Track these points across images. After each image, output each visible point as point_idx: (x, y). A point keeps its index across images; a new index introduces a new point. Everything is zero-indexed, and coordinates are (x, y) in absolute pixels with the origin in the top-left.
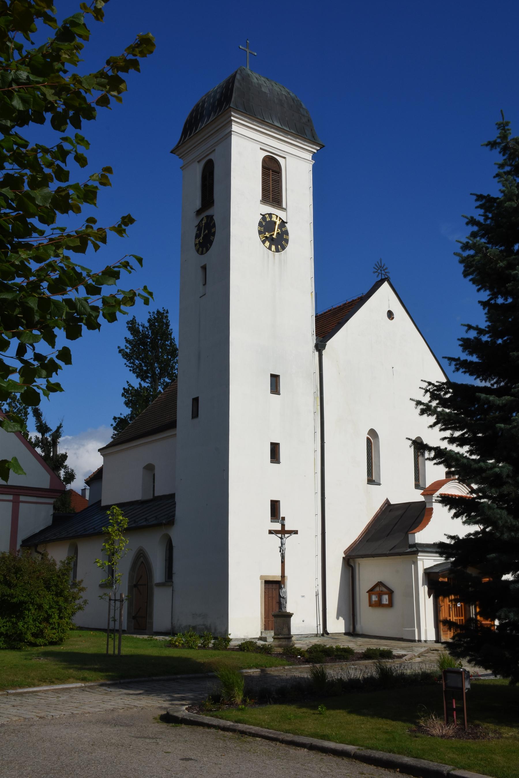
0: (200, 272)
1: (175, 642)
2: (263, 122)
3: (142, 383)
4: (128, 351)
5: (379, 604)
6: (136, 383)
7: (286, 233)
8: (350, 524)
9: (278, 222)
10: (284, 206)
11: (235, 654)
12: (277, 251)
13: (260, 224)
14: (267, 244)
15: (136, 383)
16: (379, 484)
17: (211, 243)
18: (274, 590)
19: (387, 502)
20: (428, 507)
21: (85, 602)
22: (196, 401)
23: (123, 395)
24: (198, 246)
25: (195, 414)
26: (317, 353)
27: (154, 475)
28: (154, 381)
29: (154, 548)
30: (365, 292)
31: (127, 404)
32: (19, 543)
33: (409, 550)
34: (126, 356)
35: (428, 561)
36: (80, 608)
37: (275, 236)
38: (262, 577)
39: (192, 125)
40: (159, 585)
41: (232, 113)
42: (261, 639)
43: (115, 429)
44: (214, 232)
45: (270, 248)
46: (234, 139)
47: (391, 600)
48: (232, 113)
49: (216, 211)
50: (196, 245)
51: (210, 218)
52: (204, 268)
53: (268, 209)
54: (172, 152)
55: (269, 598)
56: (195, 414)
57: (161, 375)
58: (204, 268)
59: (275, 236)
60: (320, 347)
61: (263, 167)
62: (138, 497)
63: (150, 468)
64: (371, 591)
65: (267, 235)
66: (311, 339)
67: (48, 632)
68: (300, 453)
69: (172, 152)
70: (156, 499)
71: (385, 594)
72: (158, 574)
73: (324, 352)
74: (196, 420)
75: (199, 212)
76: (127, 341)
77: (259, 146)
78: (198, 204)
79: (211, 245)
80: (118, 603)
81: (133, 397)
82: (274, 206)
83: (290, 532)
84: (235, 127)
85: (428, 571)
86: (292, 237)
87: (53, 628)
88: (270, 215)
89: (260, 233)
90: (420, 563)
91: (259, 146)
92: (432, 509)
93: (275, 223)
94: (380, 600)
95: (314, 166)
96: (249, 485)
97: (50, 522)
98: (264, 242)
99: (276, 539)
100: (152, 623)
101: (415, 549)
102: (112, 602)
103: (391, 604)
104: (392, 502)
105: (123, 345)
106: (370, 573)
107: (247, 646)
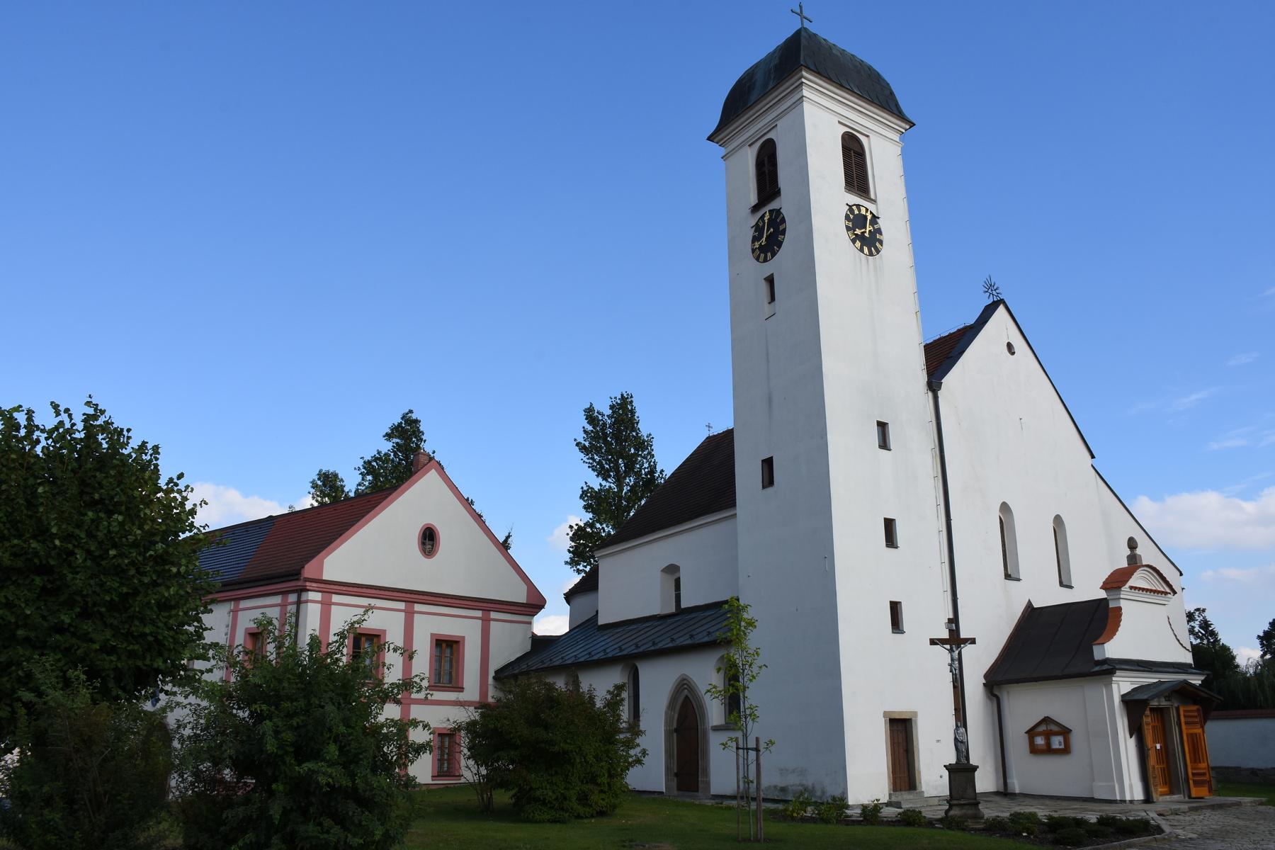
0: (764, 287)
1: (793, 811)
2: (841, 86)
3: (604, 483)
4: (587, 444)
5: (1048, 750)
6: (596, 483)
7: (879, 231)
8: (989, 633)
9: (869, 217)
10: (872, 196)
11: (860, 831)
12: (871, 254)
13: (847, 217)
14: (858, 244)
15: (596, 483)
16: (1019, 580)
17: (780, 244)
18: (901, 731)
19: (1029, 604)
20: (1112, 605)
21: (644, 752)
22: (768, 464)
23: (581, 497)
24: (758, 252)
25: (768, 479)
26: (930, 394)
27: (678, 582)
28: (619, 481)
29: (704, 674)
30: (971, 320)
31: (586, 508)
32: (491, 674)
33: (1097, 669)
34: (583, 449)
35: (1123, 684)
36: (639, 761)
37: (865, 233)
38: (885, 714)
39: (743, 100)
40: (717, 729)
41: (804, 73)
42: (889, 804)
43: (572, 539)
44: (784, 230)
45: (862, 250)
46: (807, 106)
47: (1067, 742)
48: (804, 73)
49: (784, 203)
50: (753, 251)
51: (777, 213)
52: (770, 280)
53: (854, 199)
54: (709, 139)
55: (738, 748)
56: (768, 479)
57: (627, 474)
58: (770, 280)
59: (865, 233)
60: (934, 385)
61: (843, 147)
62: (656, 610)
63: (672, 570)
64: (1032, 733)
65: (858, 232)
66: (922, 377)
67: (595, 797)
68: (921, 530)
69: (709, 139)
70: (680, 611)
71: (1057, 734)
72: (715, 712)
73: (940, 393)
74: (770, 490)
75: (755, 209)
76: (585, 432)
77: (837, 119)
78: (753, 199)
79: (779, 247)
80: (752, 754)
81: (594, 501)
82: (860, 196)
83: (966, 641)
84: (806, 92)
85: (1127, 698)
86: (885, 237)
87: (601, 791)
88: (858, 206)
89: (848, 229)
90: (1114, 686)
91: (837, 119)
92: (1120, 609)
93: (865, 217)
94: (1048, 744)
95: (903, 149)
96: (862, 578)
97: (528, 648)
98: (854, 241)
99: (942, 654)
100: (708, 783)
101: (1105, 667)
102: (741, 751)
103: (1066, 751)
104: (1037, 604)
105: (581, 437)
106: (1028, 705)
107: (871, 813)
